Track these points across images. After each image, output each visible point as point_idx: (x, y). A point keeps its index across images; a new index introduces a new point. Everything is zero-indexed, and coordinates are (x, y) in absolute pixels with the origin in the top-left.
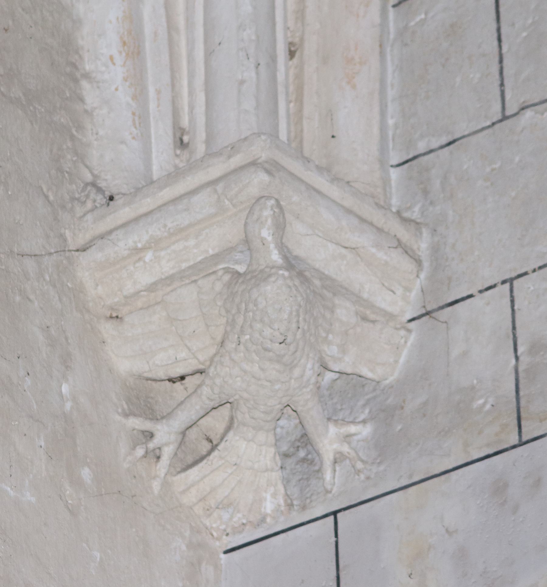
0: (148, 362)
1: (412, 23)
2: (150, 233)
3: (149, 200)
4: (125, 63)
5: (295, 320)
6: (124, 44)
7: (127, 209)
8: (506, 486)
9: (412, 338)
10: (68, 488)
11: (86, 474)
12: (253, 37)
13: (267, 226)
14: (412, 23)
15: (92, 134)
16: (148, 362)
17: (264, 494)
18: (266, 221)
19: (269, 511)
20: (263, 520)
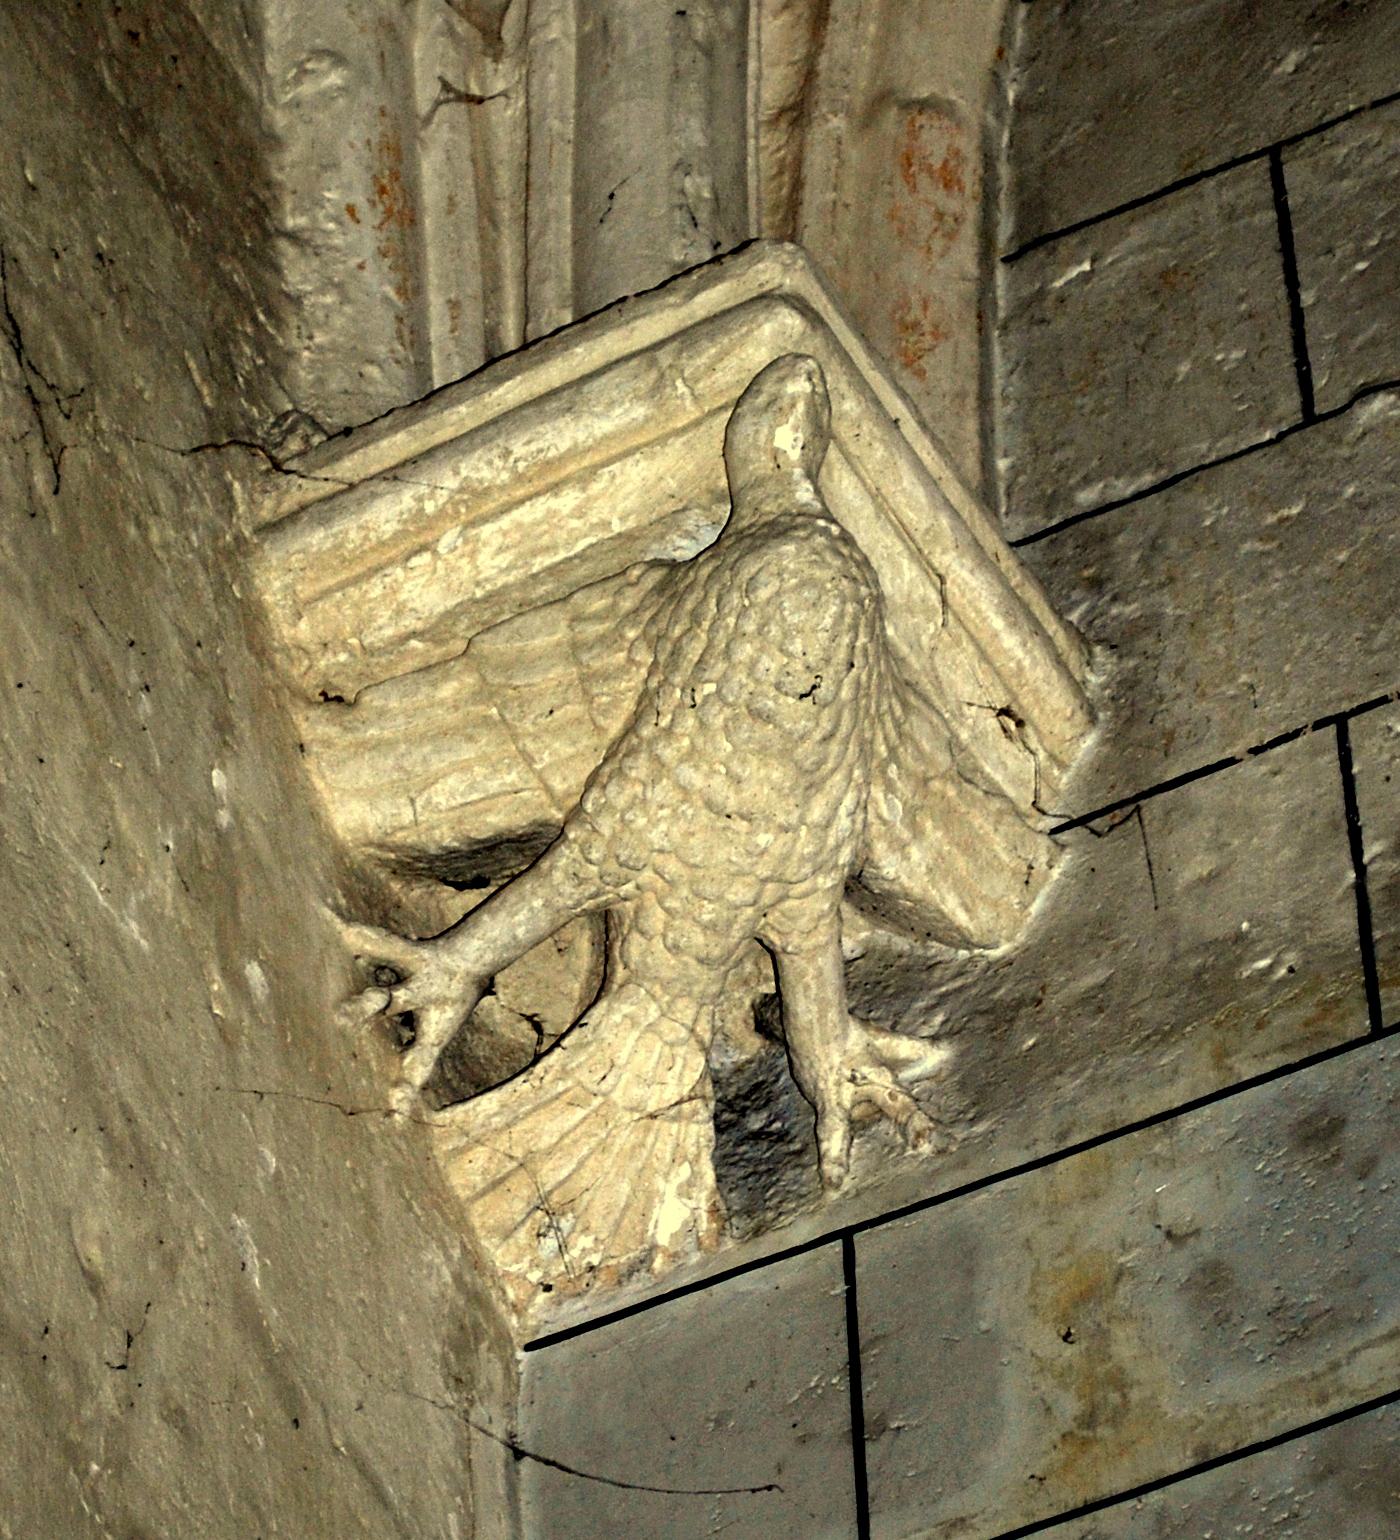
0: (412, 801)
1: (1058, 284)
2: (464, 473)
3: (463, 409)
4: (382, 224)
5: (846, 640)
6: (382, 190)
7: (400, 437)
8: (1338, 1125)
9: (1065, 860)
10: (217, 977)
11: (254, 972)
12: (706, 194)
13: (792, 420)
14: (1058, 284)
15: (299, 336)
16: (412, 801)
17: (659, 1183)
18: (793, 406)
19: (663, 1240)
20: (644, 1261)
